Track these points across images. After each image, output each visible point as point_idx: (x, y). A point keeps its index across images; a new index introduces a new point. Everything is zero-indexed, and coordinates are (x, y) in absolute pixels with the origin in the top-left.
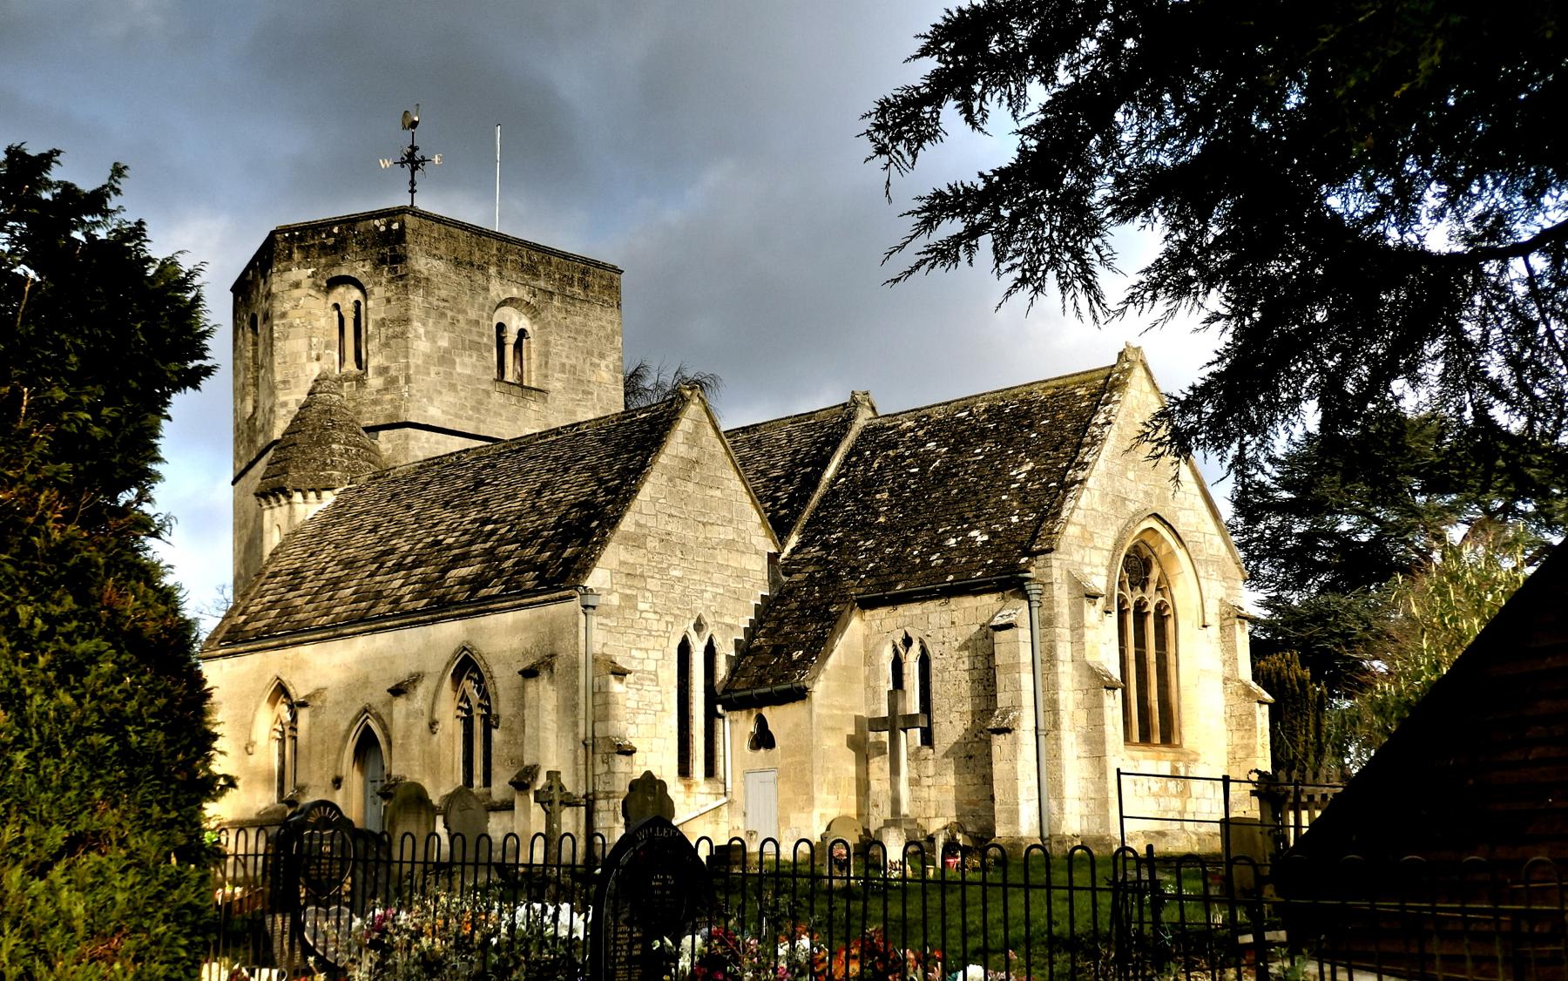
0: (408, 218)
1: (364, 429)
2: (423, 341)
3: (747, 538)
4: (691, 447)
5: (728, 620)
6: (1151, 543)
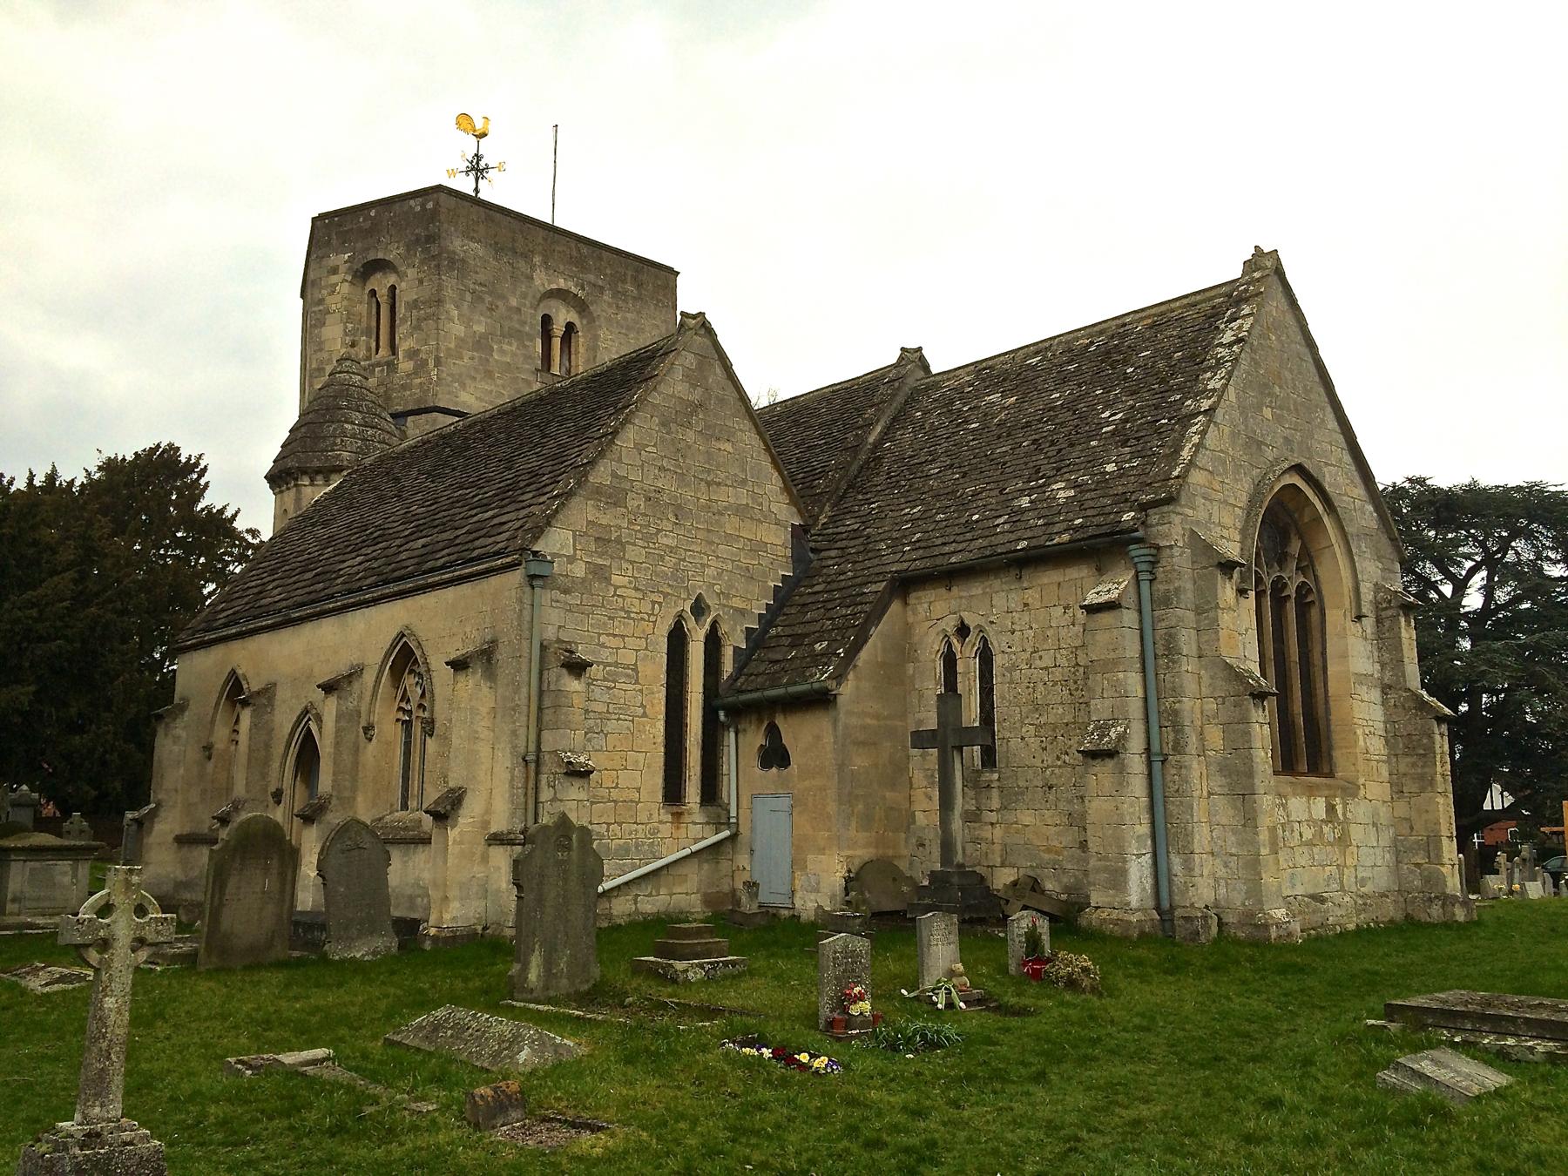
0: (443, 196)
1: (392, 415)
2: (455, 326)
3: (766, 504)
4: (694, 386)
5: (737, 603)
6: (1291, 506)
